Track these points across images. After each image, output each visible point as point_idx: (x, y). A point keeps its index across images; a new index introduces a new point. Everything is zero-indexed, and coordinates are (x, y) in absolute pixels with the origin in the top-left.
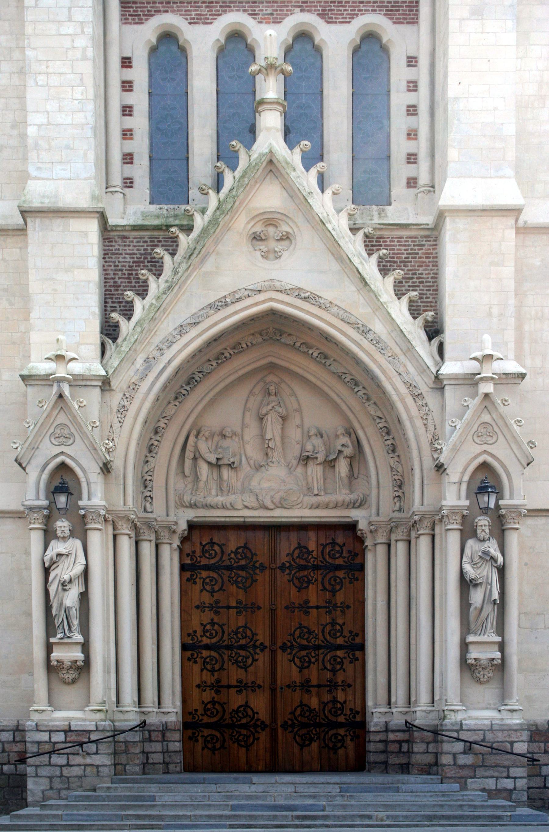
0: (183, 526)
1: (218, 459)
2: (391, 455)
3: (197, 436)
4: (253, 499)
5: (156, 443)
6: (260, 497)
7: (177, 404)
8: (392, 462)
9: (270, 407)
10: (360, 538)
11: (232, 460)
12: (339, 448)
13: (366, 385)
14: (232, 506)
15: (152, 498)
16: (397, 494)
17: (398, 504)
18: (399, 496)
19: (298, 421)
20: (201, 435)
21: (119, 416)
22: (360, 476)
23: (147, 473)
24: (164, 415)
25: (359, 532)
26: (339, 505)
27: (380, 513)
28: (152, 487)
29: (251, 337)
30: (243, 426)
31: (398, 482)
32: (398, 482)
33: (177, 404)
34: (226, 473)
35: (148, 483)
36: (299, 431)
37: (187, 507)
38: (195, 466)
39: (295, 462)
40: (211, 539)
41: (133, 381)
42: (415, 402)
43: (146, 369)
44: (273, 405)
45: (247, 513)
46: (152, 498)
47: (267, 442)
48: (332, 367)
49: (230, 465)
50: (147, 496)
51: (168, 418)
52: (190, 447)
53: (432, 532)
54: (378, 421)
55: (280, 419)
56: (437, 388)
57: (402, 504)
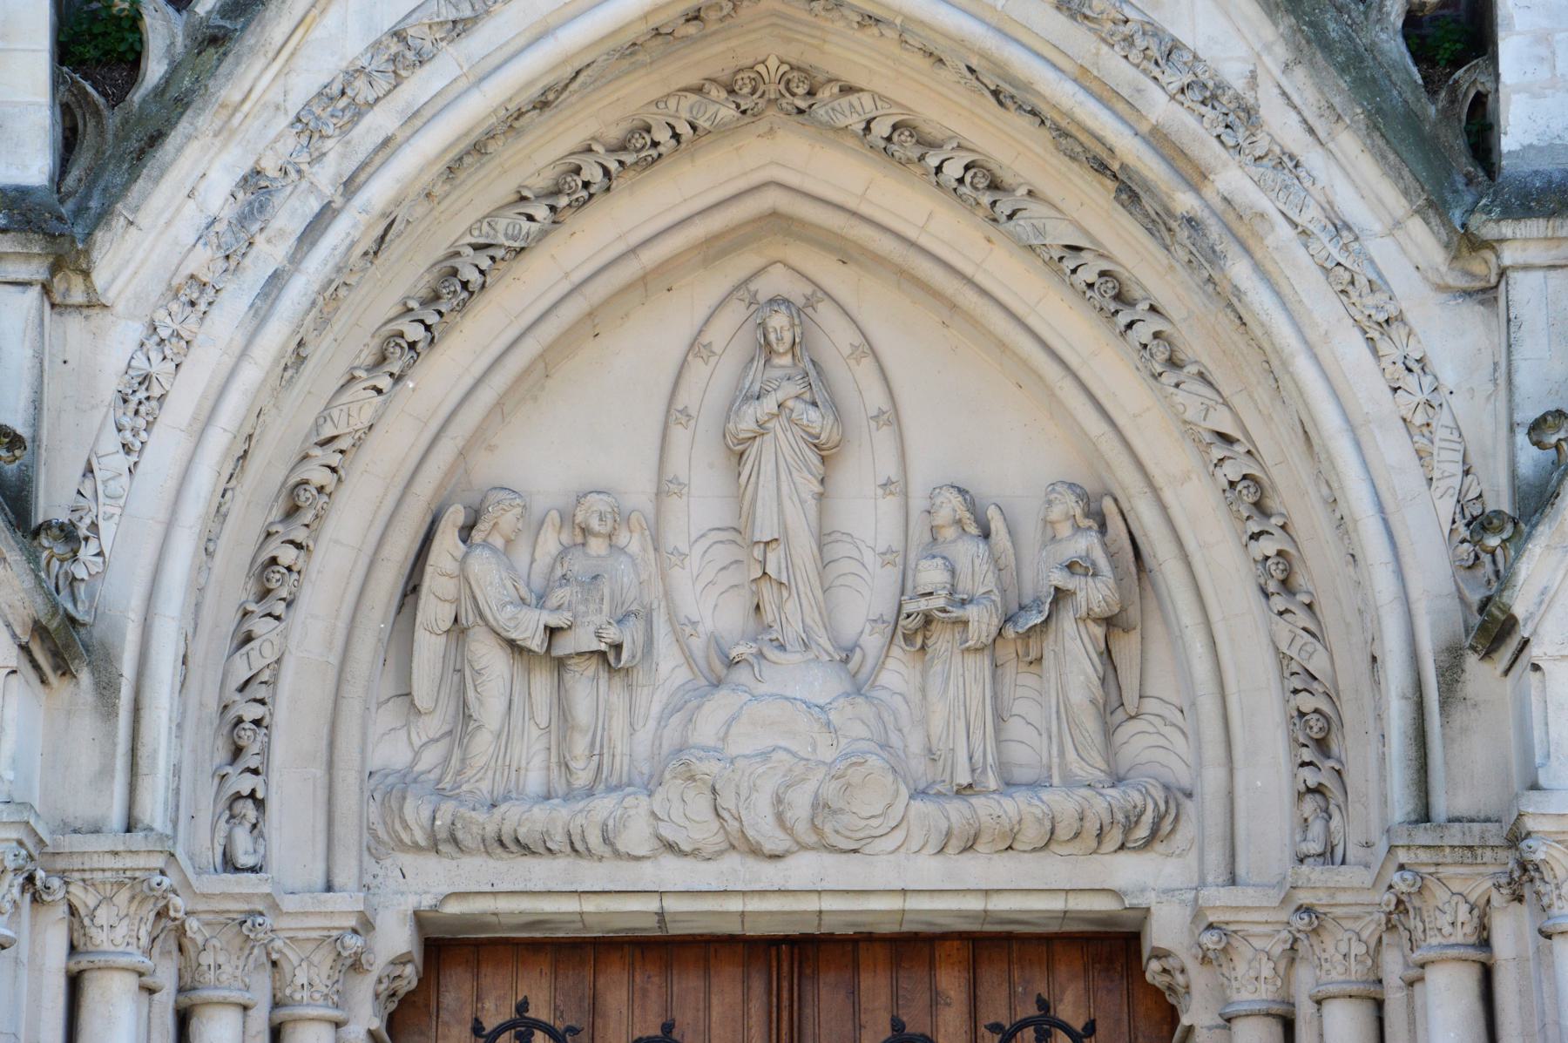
0: (396, 938)
1: (552, 632)
2: (1279, 603)
3: (466, 532)
4: (700, 805)
5: (288, 555)
6: (727, 801)
7: (384, 382)
8: (1282, 628)
9: (769, 404)
10: (1157, 992)
11: (612, 634)
12: (1059, 578)
13: (1163, 299)
14: (606, 840)
15: (260, 804)
16: (1311, 777)
17: (1317, 828)
18: (1318, 790)
19: (888, 467)
20: (483, 527)
21: (126, 421)
22: (1150, 705)
23: (242, 689)
24: (328, 432)
25: (1155, 966)
26: (1063, 833)
27: (1241, 870)
28: (265, 752)
29: (693, 98)
30: (664, 487)
31: (1316, 723)
32: (1316, 723)
33: (384, 382)
34: (585, 688)
35: (246, 734)
36: (889, 506)
37: (417, 847)
38: (459, 673)
39: (873, 643)
40: (522, 1007)
41: (191, 267)
42: (1375, 351)
43: (243, 220)
44: (780, 395)
45: (673, 873)
46: (260, 804)
47: (758, 552)
48: (1021, 225)
49: (603, 654)
50: (238, 796)
51: (343, 444)
52: (437, 582)
53: (1481, 956)
54: (1218, 452)
55: (813, 459)
56: (1467, 293)
57: (1336, 822)
